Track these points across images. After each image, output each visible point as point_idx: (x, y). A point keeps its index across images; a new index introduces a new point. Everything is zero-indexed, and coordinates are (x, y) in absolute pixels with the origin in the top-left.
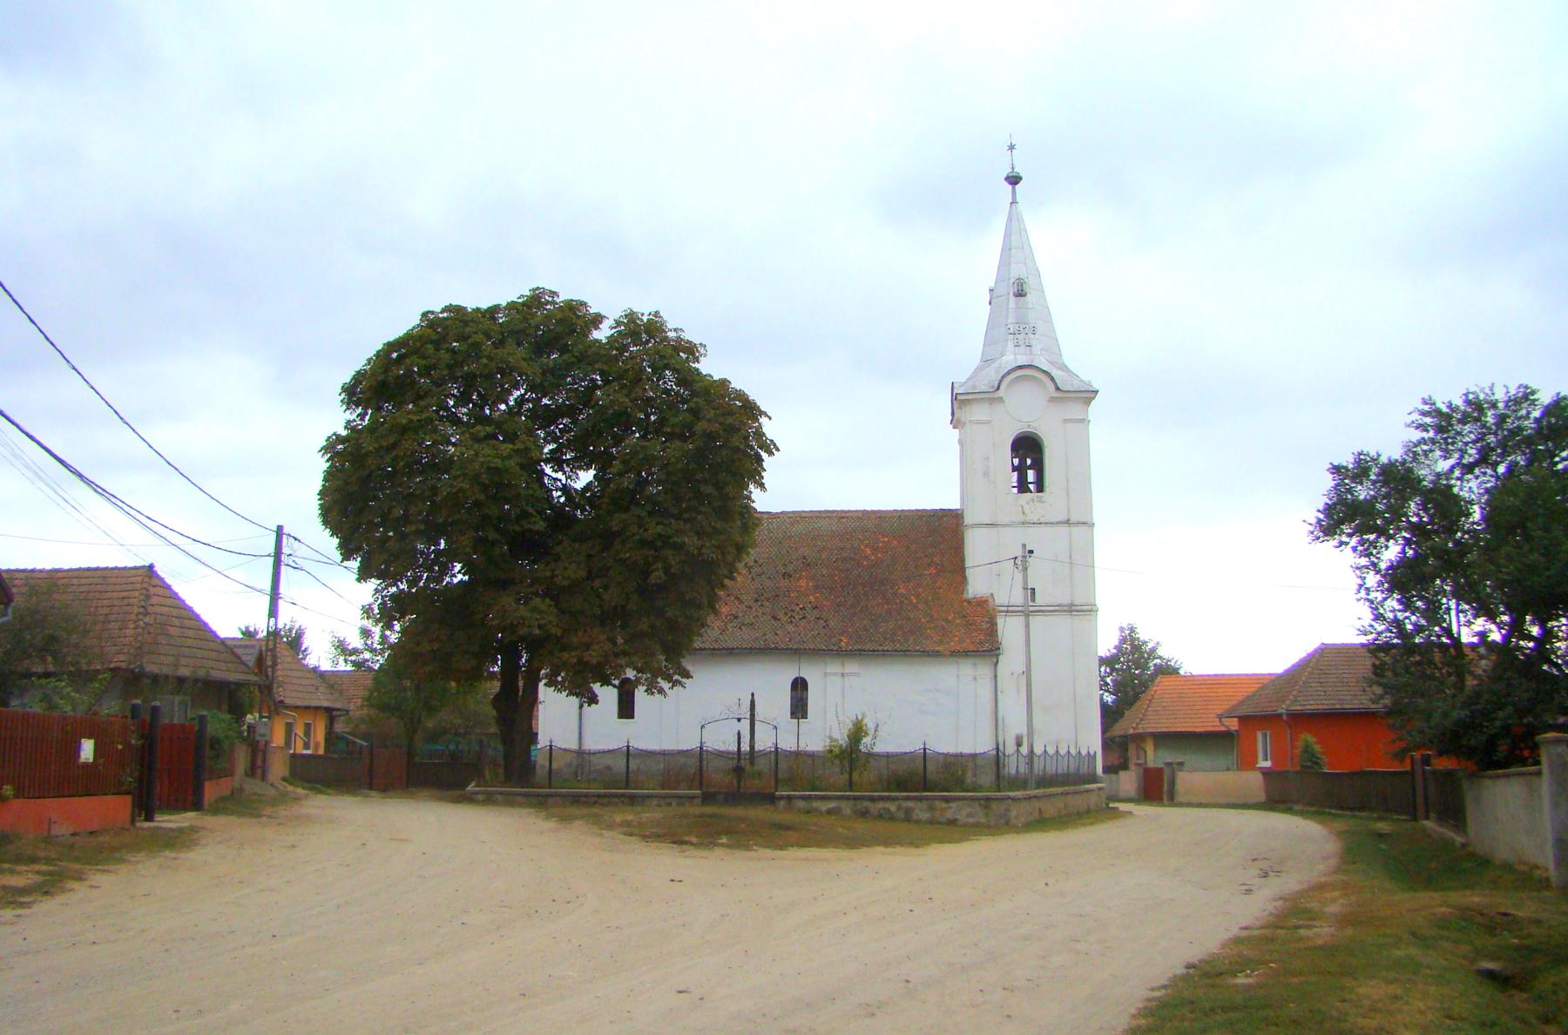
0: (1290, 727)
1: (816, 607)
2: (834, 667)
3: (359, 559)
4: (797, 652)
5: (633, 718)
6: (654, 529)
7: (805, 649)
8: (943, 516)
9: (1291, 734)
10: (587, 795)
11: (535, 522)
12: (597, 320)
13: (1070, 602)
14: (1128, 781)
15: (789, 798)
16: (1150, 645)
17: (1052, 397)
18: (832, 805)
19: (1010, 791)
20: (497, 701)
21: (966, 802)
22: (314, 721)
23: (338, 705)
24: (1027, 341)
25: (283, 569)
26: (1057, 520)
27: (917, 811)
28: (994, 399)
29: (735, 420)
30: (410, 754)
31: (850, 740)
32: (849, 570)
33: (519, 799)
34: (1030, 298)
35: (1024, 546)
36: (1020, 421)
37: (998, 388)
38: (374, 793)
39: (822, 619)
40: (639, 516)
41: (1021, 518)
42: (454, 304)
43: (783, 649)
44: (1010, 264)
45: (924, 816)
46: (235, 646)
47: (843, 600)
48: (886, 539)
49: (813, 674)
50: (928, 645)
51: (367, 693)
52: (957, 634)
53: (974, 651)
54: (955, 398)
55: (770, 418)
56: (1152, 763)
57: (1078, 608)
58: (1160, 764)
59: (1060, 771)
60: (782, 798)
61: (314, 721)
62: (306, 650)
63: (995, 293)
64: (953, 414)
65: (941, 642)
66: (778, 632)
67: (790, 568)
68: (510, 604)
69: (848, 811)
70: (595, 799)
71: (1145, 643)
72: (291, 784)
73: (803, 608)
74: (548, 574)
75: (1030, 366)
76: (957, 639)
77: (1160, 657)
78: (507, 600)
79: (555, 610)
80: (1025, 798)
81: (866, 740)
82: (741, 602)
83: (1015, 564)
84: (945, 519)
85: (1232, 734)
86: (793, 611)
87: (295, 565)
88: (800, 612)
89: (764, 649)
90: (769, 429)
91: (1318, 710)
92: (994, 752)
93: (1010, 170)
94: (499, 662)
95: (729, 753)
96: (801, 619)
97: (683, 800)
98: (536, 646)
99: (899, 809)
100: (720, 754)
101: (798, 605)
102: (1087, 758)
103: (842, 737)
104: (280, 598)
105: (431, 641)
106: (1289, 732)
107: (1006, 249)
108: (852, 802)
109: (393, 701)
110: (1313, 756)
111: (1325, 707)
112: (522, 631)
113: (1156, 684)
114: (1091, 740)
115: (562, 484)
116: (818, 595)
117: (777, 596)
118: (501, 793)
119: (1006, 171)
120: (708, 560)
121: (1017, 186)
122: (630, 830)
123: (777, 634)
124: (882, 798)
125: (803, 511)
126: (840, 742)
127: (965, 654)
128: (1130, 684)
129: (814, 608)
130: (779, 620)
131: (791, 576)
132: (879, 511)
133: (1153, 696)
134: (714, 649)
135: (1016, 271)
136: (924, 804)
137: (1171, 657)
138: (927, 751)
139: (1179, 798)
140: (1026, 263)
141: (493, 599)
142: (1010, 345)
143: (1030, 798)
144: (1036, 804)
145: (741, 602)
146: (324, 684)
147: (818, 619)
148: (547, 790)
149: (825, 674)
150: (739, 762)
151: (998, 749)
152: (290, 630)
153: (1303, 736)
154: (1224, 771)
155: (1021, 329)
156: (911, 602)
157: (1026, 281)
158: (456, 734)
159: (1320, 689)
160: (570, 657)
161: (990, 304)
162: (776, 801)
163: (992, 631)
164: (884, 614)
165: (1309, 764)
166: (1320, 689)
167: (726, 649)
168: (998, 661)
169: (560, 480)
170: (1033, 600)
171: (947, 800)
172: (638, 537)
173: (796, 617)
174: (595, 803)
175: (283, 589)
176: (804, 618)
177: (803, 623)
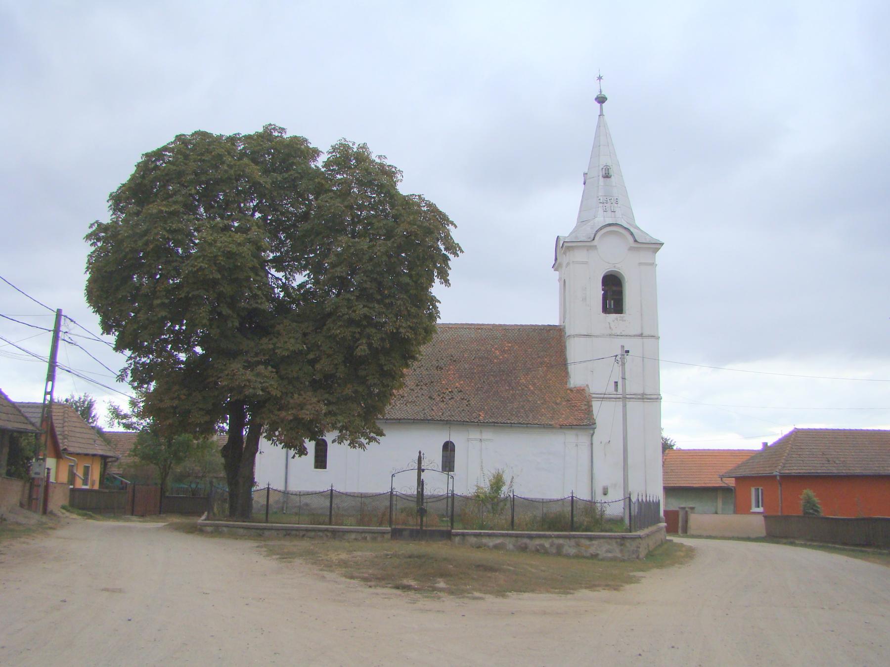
0: (781, 484)
1: (461, 391)
3: (117, 333)
4: (447, 423)
5: (326, 468)
6: (361, 309)
7: (450, 420)
8: (549, 330)
9: (781, 491)
10: (297, 530)
11: (261, 303)
12: (316, 153)
13: (642, 392)
15: (463, 535)
17: (631, 247)
18: (498, 541)
20: (226, 451)
21: (605, 540)
22: (92, 465)
23: (109, 454)
24: (612, 208)
25: (61, 343)
26: (634, 334)
28: (591, 246)
29: (430, 224)
30: (163, 491)
31: (492, 488)
32: (484, 365)
33: (241, 531)
35: (623, 347)
36: (609, 263)
37: (594, 240)
38: (134, 518)
39: (466, 400)
40: (349, 300)
42: (202, 130)
43: (437, 420)
44: (599, 155)
45: (573, 551)
46: (20, 406)
47: (480, 386)
48: (510, 345)
49: (459, 439)
51: (133, 447)
53: (577, 425)
57: (649, 396)
60: (457, 535)
61: (92, 465)
62: (94, 417)
63: (588, 176)
64: (556, 259)
65: (552, 418)
66: (434, 408)
68: (238, 369)
69: (511, 546)
72: (68, 511)
73: (452, 392)
74: (271, 346)
75: (616, 225)
76: (564, 416)
78: (236, 366)
79: (276, 376)
81: (505, 489)
83: (616, 360)
84: (551, 331)
85: (732, 490)
87: (70, 341)
88: (449, 394)
90: (456, 235)
91: (799, 473)
93: (599, 93)
94: (228, 421)
95: (410, 496)
96: (450, 399)
97: (376, 535)
98: (259, 405)
99: (552, 545)
100: (405, 497)
101: (447, 389)
103: (486, 485)
104: (57, 366)
105: (172, 399)
106: (780, 488)
107: (597, 146)
108: (513, 539)
109: (152, 453)
110: (814, 505)
111: (804, 471)
112: (248, 392)
115: (282, 282)
116: (462, 382)
117: (432, 382)
118: (227, 526)
119: (596, 94)
120: (405, 337)
121: (603, 105)
122: (350, 570)
123: (432, 409)
124: (540, 537)
127: (571, 427)
129: (459, 392)
130: (434, 399)
131: (442, 369)
132: (505, 325)
135: (604, 161)
138: (574, 498)
139: (691, 531)
140: (610, 156)
141: (225, 365)
142: (600, 211)
146: (100, 438)
147: (463, 399)
148: (265, 524)
149: (468, 440)
152: (84, 402)
153: (805, 491)
154: (714, 514)
156: (529, 390)
157: (611, 167)
158: (197, 477)
159: (799, 459)
160: (287, 415)
161: (585, 184)
162: (452, 537)
163: (589, 411)
165: (811, 511)
166: (799, 459)
167: (396, 419)
168: (594, 433)
169: (281, 280)
171: (591, 538)
173: (447, 397)
175: (60, 359)
176: (452, 398)
177: (451, 402)
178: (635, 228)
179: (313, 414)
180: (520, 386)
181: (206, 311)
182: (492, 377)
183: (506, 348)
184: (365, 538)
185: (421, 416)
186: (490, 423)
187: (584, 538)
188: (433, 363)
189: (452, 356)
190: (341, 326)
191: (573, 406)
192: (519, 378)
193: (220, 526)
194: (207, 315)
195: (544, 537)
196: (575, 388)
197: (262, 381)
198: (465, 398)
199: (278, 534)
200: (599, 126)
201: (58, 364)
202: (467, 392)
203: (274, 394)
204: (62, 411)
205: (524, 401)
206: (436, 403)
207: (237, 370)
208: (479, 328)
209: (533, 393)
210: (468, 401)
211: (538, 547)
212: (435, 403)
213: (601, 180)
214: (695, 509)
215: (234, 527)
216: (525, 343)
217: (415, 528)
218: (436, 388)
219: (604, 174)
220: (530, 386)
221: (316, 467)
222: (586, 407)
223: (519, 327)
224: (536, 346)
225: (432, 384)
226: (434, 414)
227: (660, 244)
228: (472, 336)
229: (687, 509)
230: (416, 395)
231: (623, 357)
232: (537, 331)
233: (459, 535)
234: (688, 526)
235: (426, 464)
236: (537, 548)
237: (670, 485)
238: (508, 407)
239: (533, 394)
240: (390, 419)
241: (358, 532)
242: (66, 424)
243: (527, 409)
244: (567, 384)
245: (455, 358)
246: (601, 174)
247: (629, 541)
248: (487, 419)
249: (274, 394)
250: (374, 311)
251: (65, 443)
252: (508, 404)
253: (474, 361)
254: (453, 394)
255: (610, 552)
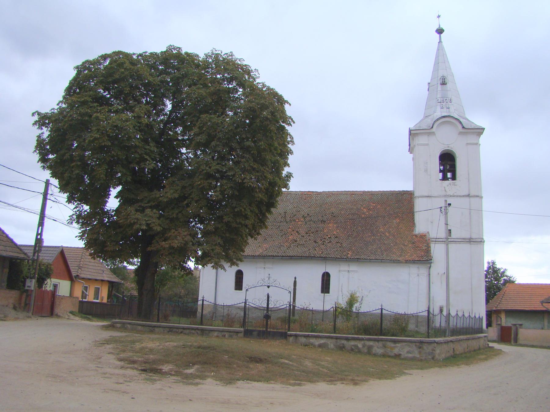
1: (337, 237)
2: (344, 267)
4: (324, 259)
10: (177, 328)
13: (469, 237)
14: (493, 332)
15: (296, 336)
16: (502, 270)
18: (322, 341)
19: (435, 337)
24: (447, 106)
25: (48, 202)
27: (375, 348)
33: (140, 328)
34: (449, 86)
37: (432, 128)
39: (340, 243)
41: (444, 193)
43: (318, 257)
44: (438, 70)
45: (380, 351)
47: (351, 234)
48: (374, 205)
49: (333, 270)
50: (395, 257)
52: (409, 251)
54: (410, 134)
55: (290, 105)
56: (504, 324)
58: (509, 325)
59: (458, 326)
63: (431, 85)
64: (410, 145)
65: (401, 255)
66: (316, 249)
67: (325, 219)
69: (332, 346)
70: (182, 330)
71: (499, 269)
76: (409, 254)
77: (506, 276)
80: (445, 342)
81: (356, 305)
82: (299, 234)
83: (441, 210)
86: (325, 239)
88: (328, 239)
89: (308, 257)
92: (426, 314)
96: (328, 243)
97: (232, 334)
99: (364, 346)
101: (327, 236)
102: (478, 320)
103: (343, 303)
107: (437, 63)
108: (334, 340)
113: (506, 287)
114: (481, 311)
117: (317, 231)
118: (130, 324)
123: (315, 250)
125: (333, 191)
126: (342, 306)
127: (414, 262)
128: (492, 287)
129: (336, 238)
130: (317, 243)
131: (325, 222)
132: (371, 192)
133: (504, 293)
134: (283, 256)
136: (380, 344)
137: (511, 276)
139: (520, 341)
142: (438, 108)
143: (447, 342)
144: (451, 345)
145: (299, 234)
149: (340, 271)
150: (268, 312)
151: (429, 311)
155: (444, 100)
161: (428, 91)
162: (288, 337)
163: (428, 251)
164: (371, 241)
167: (289, 257)
170: (450, 236)
171: (395, 342)
172: (205, 171)
173: (326, 241)
174: (181, 332)
175: (48, 212)
177: (329, 245)
178: (464, 119)
179: (181, 243)
180: (379, 233)
181: (103, 169)
182: (359, 227)
183: (371, 207)
184: (224, 336)
185: (307, 254)
186: (355, 259)
187: (390, 341)
188: (319, 218)
189: (333, 213)
190: (201, 179)
191: (416, 247)
192: (379, 228)
193: (298, 336)
194: (104, 171)
195: (358, 340)
196: (419, 234)
197: (147, 220)
198: (340, 242)
199: (164, 331)
200: (438, 50)
201: (46, 215)
202: (341, 238)
203: (155, 229)
204: (82, 252)
205: (381, 244)
206: (319, 245)
207: (130, 212)
208: (352, 193)
209: (388, 238)
210: (341, 244)
211: (353, 347)
212: (318, 245)
213: (439, 86)
214: (523, 326)
215: (134, 324)
216: (385, 203)
217: (261, 329)
218: (319, 235)
219: (441, 82)
220: (387, 233)
221: (236, 289)
222: (426, 248)
223: (382, 193)
224: (393, 205)
225: (317, 232)
226: (316, 253)
227: (482, 129)
228: (348, 199)
229: (517, 326)
230: (305, 240)
231: (446, 208)
232: (394, 195)
233: (293, 336)
234: (518, 337)
235: (271, 282)
236: (352, 347)
237: (508, 309)
238: (369, 248)
239: (388, 239)
240: (285, 256)
241: (220, 331)
242: (82, 260)
243: (383, 249)
244: (413, 232)
245: (335, 214)
246: (439, 82)
247: (426, 344)
248: (353, 256)
249: (155, 229)
250: (225, 167)
251: (79, 272)
252: (370, 246)
253: (348, 217)
254: (331, 239)
255: (410, 353)
